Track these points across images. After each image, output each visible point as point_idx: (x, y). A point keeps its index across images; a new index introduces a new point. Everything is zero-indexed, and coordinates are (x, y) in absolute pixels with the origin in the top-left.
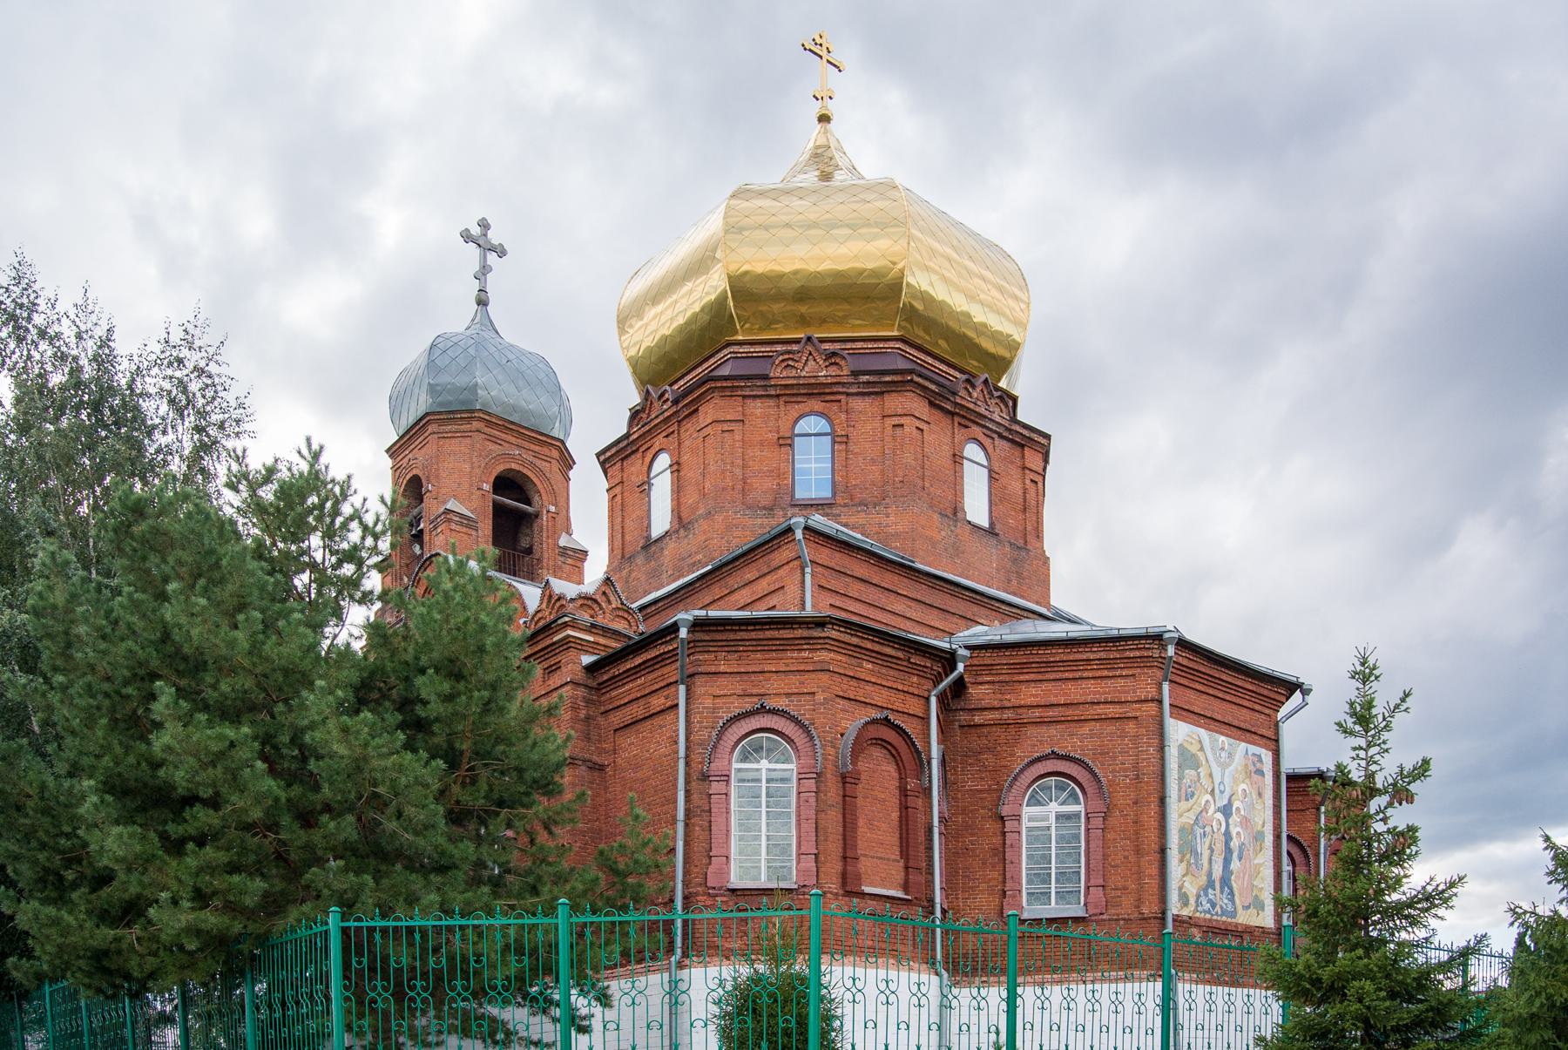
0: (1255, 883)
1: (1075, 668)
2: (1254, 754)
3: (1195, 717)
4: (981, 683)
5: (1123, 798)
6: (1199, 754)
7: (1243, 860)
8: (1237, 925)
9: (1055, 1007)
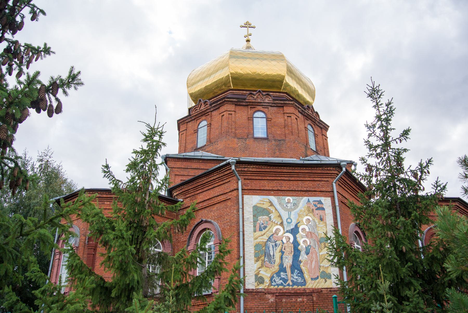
0: (321, 265)
1: (211, 184)
4: (187, 198)
6: (270, 208)
7: (310, 254)
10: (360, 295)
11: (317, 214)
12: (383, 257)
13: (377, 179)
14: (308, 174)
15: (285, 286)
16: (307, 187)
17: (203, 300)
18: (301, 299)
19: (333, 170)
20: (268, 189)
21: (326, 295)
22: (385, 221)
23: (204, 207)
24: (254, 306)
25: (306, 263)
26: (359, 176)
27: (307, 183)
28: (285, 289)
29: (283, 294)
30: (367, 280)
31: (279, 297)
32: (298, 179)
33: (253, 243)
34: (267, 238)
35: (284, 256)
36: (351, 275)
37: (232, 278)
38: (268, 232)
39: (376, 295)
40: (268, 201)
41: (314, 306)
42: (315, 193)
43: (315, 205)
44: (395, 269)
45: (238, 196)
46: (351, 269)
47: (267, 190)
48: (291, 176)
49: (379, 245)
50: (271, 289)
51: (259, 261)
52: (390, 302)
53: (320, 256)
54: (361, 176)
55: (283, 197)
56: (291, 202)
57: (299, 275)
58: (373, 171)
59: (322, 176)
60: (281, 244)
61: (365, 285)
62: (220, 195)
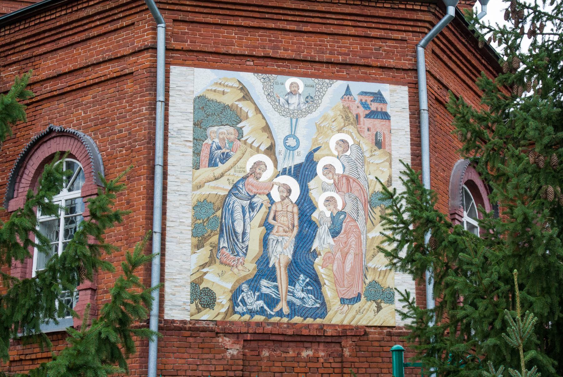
0: (371, 265)
1: (81, 29)
3: (234, 60)
4: (10, 65)
6: (240, 104)
7: (341, 236)
10: (462, 346)
11: (369, 130)
12: (530, 251)
13: (535, 41)
14: (352, 18)
15: (271, 316)
16: (345, 54)
17: (41, 347)
18: (310, 353)
19: (421, 11)
20: (238, 52)
21: (377, 344)
22: (542, 158)
23: (58, 92)
24: (186, 367)
25: (330, 259)
26: (485, 30)
27: (348, 41)
28: (269, 324)
29: (265, 337)
30: (481, 308)
31: (254, 344)
32: (324, 29)
33: (189, 197)
34: (230, 187)
35: (271, 237)
36: (442, 296)
37: (122, 288)
38: (233, 170)
39: (503, 349)
40: (237, 85)
41: (345, 370)
42: (368, 71)
43: (365, 105)
44: (557, 285)
45: (154, 66)
46: (442, 278)
47: (235, 55)
48: (305, 19)
49: (519, 220)
50: (232, 323)
51: (203, 246)
52: (534, 369)
53: (369, 241)
54: (491, 30)
55: (280, 78)
56: (300, 91)
57: (309, 288)
58: (524, 20)
59: (388, 27)
60: (267, 204)
61: (475, 322)
62: (105, 62)
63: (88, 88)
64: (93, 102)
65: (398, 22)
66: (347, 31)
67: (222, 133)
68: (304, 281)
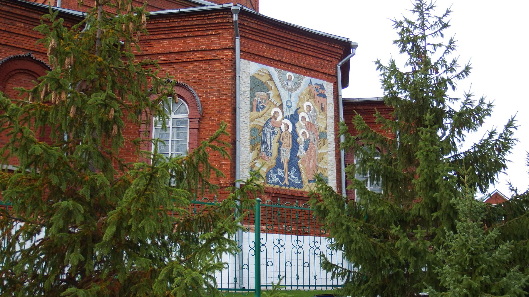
0: (319, 165)
1: (185, 31)
2: (316, 84)
3: (266, 60)
5: (212, 109)
6: (269, 82)
7: (308, 150)
8: (302, 193)
9: (288, 251)
23: (169, 61)
32: (300, 50)
33: (249, 125)
35: (281, 148)
43: (318, 91)
48: (294, 45)
50: (267, 188)
51: (254, 150)
55: (284, 72)
56: (292, 79)
57: (296, 174)
63: (190, 63)
64: (193, 70)
65: (330, 52)
66: (309, 53)
67: (262, 95)
68: (294, 170)
